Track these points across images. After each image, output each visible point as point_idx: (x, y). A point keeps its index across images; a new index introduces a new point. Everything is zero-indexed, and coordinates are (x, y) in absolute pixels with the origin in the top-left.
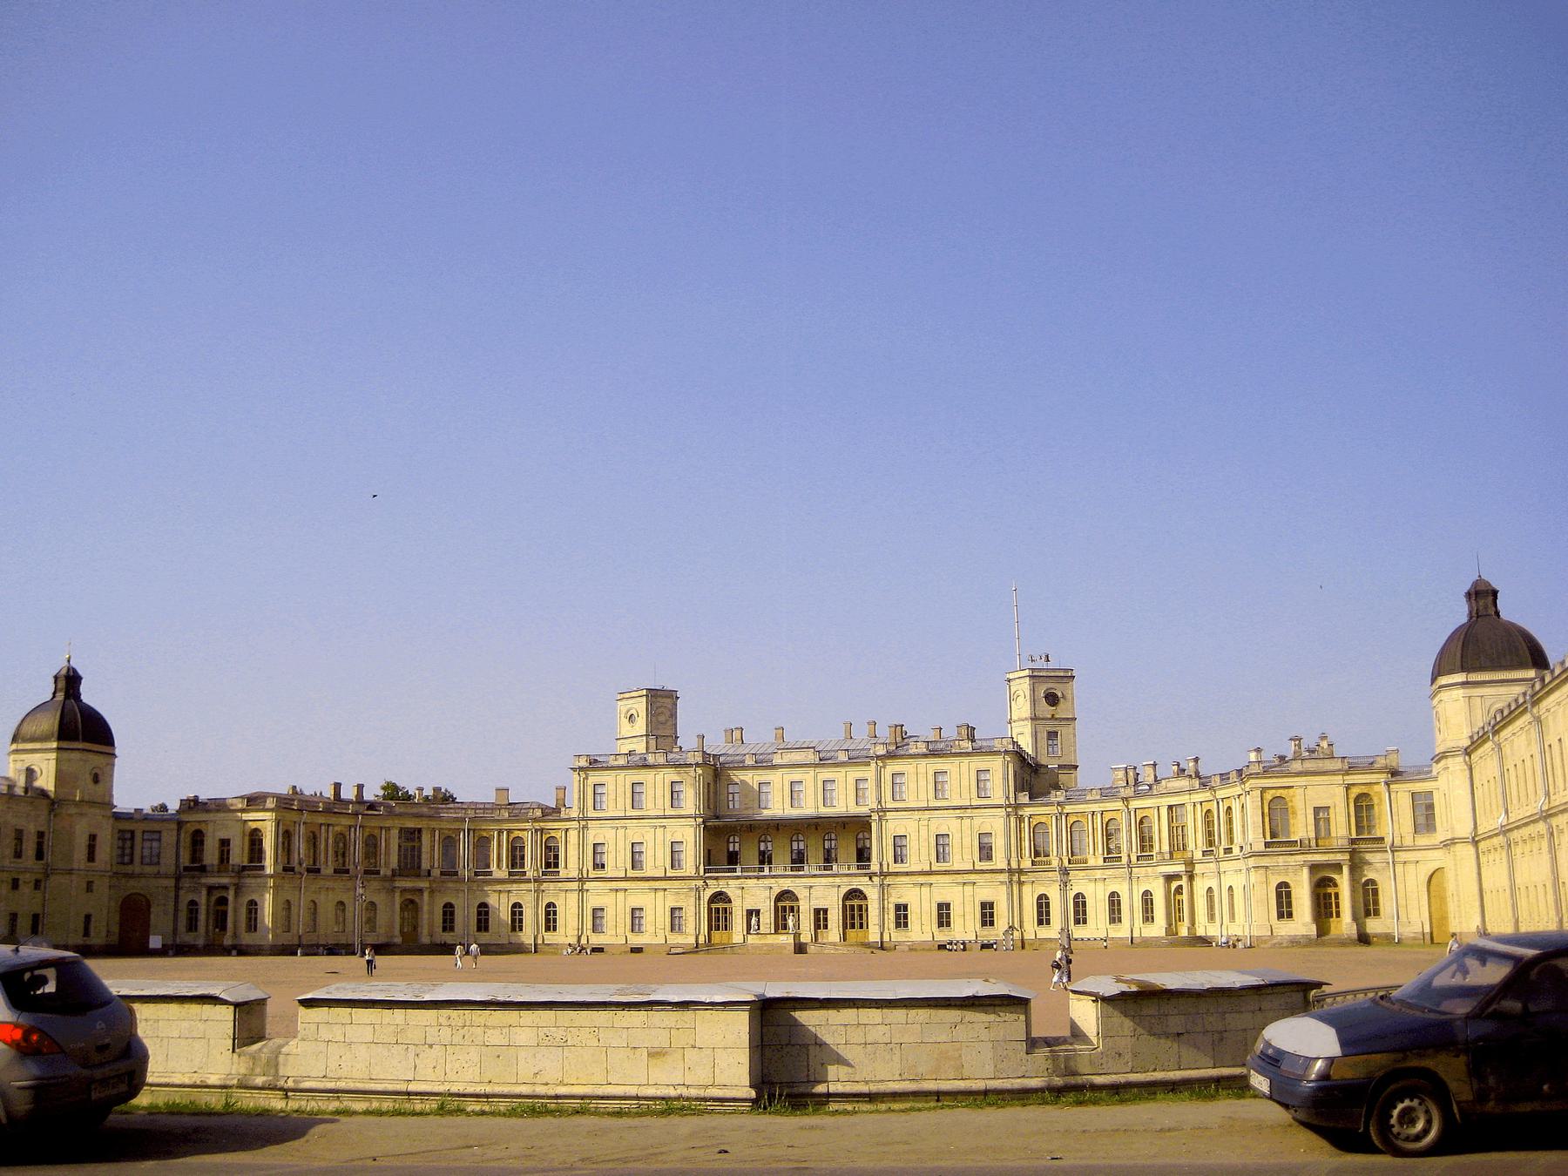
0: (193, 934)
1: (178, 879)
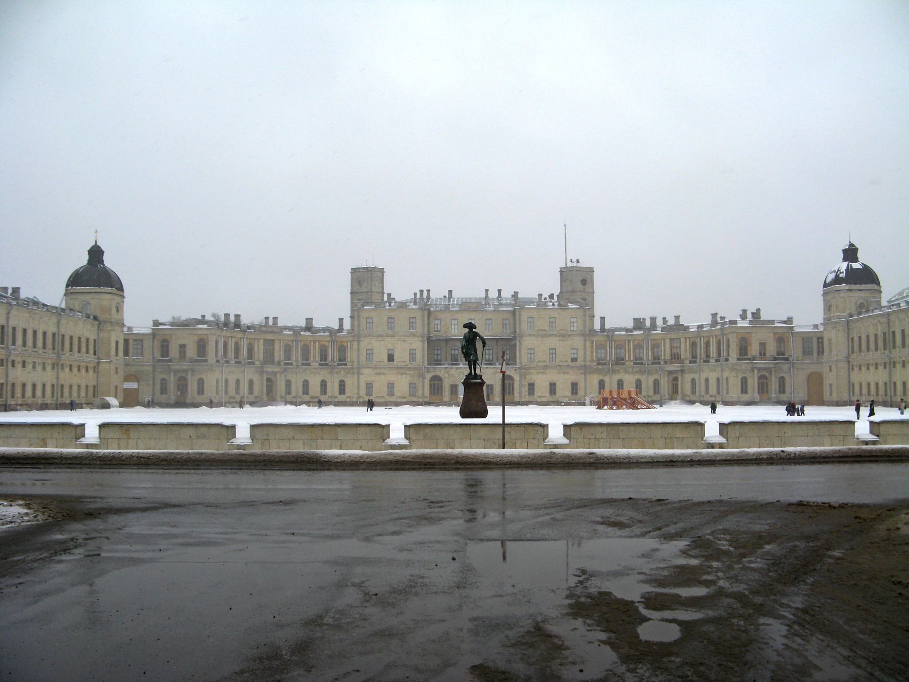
0: (164, 396)
1: (154, 366)
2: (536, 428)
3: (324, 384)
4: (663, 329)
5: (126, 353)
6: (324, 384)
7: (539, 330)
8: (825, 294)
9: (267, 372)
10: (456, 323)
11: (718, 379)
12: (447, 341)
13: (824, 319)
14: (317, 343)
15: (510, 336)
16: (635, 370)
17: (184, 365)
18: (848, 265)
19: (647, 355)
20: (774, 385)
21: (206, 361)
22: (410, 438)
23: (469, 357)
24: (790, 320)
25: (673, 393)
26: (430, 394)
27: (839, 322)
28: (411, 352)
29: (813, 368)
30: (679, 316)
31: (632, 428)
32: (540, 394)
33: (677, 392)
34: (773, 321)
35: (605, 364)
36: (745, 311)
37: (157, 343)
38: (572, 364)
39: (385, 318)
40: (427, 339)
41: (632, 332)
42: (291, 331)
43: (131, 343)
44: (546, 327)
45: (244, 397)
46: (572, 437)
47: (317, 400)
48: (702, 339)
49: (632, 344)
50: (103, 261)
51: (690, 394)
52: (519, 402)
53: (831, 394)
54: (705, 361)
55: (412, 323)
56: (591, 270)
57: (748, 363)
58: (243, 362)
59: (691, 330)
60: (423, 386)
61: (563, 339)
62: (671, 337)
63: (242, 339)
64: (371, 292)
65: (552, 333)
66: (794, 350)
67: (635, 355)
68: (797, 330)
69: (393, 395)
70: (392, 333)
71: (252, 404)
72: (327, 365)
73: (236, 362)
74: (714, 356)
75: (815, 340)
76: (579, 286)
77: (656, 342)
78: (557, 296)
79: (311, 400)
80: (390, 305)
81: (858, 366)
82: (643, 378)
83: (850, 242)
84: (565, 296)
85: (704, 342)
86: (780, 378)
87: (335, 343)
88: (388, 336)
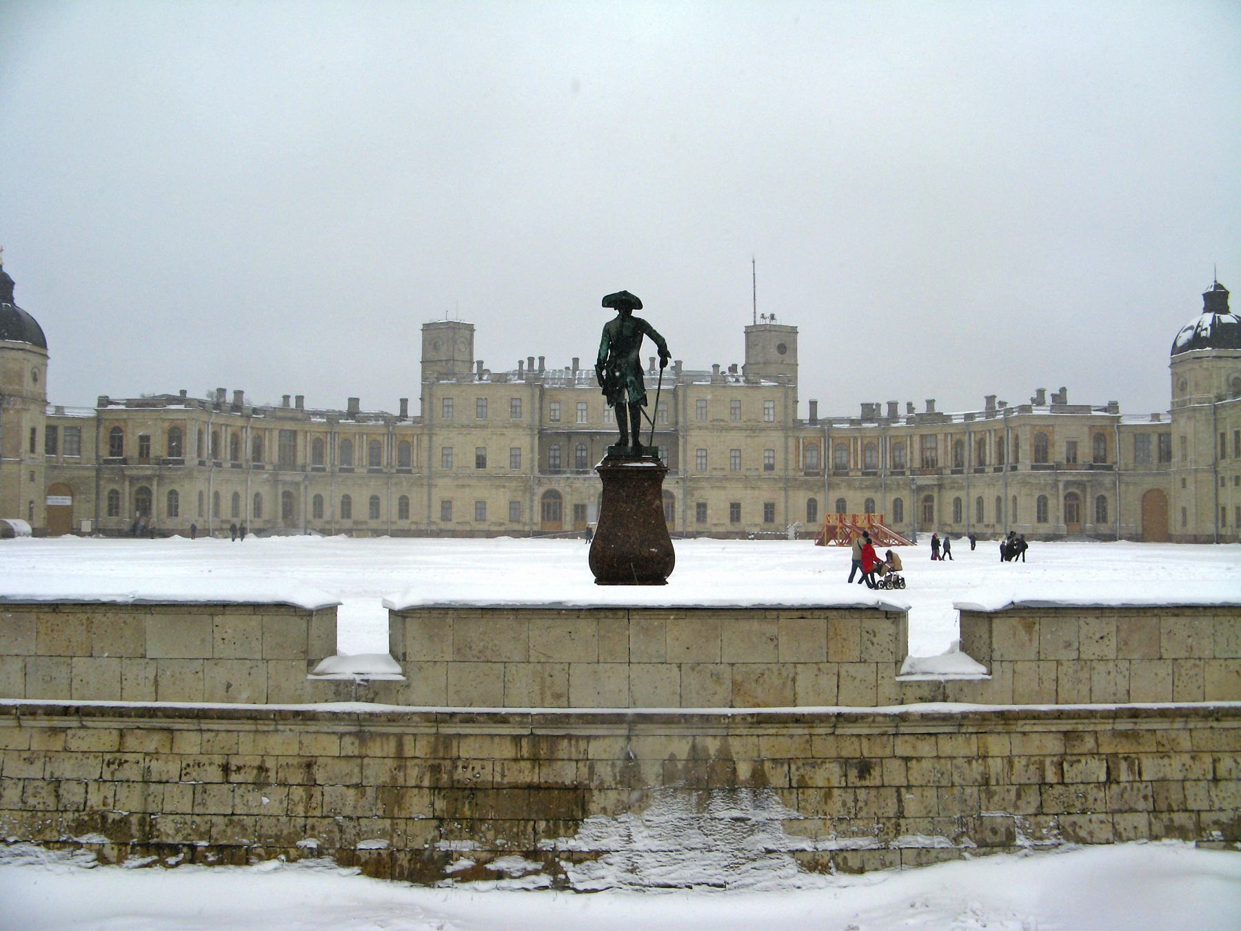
0: (114, 519)
1: (98, 471)
2: (869, 624)
3: (375, 502)
4: (909, 420)
5: (51, 448)
6: (375, 502)
7: (714, 420)
8: (1173, 365)
9: (285, 483)
10: (584, 407)
11: (999, 499)
12: (569, 435)
13: (1173, 403)
14: (365, 436)
15: (668, 429)
16: (865, 483)
17: (147, 468)
18: (1214, 317)
19: (883, 461)
20: (1089, 509)
21: (182, 462)
22: (404, 654)
23: (621, 393)
24: (1113, 407)
25: (925, 521)
26: (543, 518)
27: (1201, 409)
28: (513, 453)
29: (1149, 483)
30: (934, 401)
31: (1204, 623)
32: (715, 522)
33: (931, 520)
34: (1087, 408)
35: (818, 474)
36: (1041, 392)
37: (104, 434)
38: (766, 474)
39: (473, 399)
40: (539, 433)
41: (860, 424)
42: (323, 418)
43: (61, 433)
44: (725, 415)
45: (246, 521)
46: (996, 655)
47: (228, 526)
48: (973, 435)
49: (859, 443)
50: (13, 298)
51: (892, 523)
53: (1184, 523)
54: (976, 471)
55: (514, 409)
56: (793, 331)
57: (1050, 474)
58: (244, 465)
59: (955, 421)
60: (532, 507)
61: (752, 435)
62: (921, 433)
63: (244, 430)
64: (454, 360)
65: (734, 424)
66: (1121, 454)
67: (864, 461)
68: (1126, 421)
69: (485, 520)
70: (483, 423)
71: (260, 532)
72: (380, 471)
73: (233, 466)
74: (993, 463)
75: (1154, 439)
76: (774, 353)
77: (898, 441)
78: (742, 368)
79: (355, 527)
80: (481, 379)
81: (1233, 478)
82: (877, 497)
83: (1216, 281)
84: (753, 369)
85: (975, 441)
86: (1098, 498)
87: (394, 437)
88: (476, 427)
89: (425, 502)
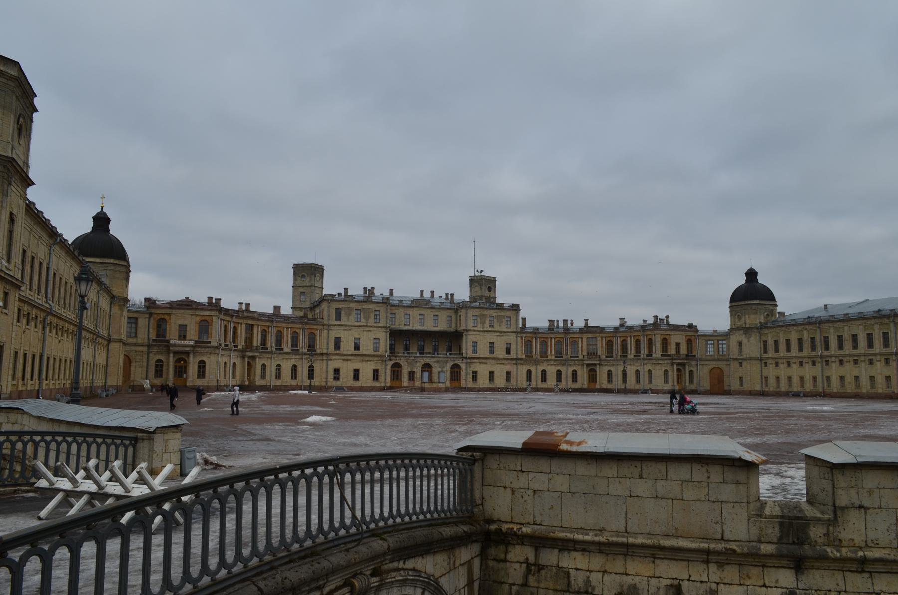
52: (465, 388)
89: (324, 369)
